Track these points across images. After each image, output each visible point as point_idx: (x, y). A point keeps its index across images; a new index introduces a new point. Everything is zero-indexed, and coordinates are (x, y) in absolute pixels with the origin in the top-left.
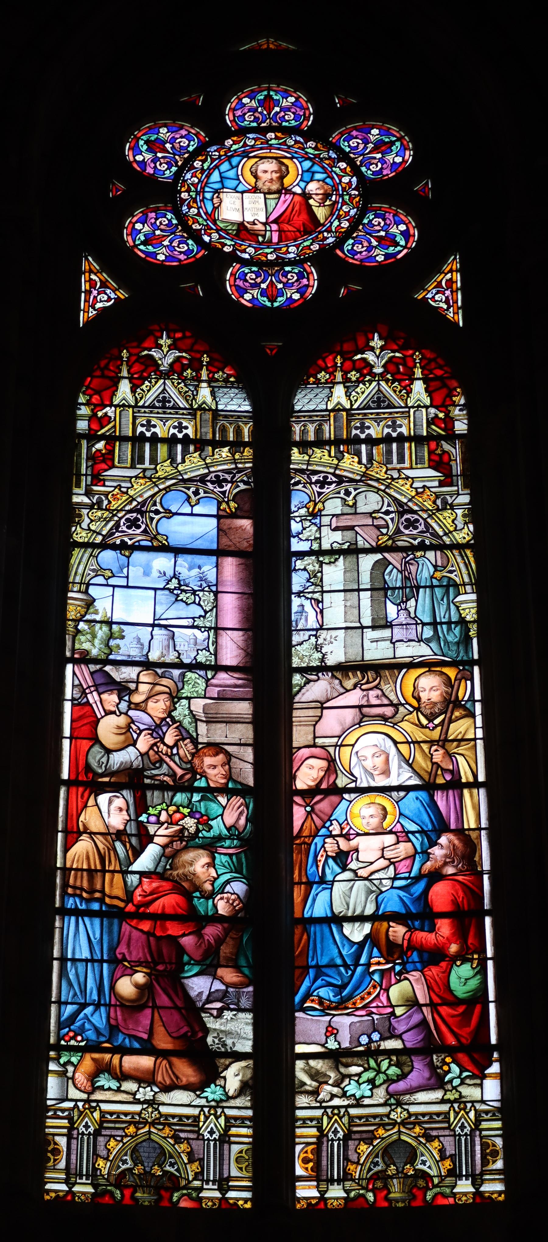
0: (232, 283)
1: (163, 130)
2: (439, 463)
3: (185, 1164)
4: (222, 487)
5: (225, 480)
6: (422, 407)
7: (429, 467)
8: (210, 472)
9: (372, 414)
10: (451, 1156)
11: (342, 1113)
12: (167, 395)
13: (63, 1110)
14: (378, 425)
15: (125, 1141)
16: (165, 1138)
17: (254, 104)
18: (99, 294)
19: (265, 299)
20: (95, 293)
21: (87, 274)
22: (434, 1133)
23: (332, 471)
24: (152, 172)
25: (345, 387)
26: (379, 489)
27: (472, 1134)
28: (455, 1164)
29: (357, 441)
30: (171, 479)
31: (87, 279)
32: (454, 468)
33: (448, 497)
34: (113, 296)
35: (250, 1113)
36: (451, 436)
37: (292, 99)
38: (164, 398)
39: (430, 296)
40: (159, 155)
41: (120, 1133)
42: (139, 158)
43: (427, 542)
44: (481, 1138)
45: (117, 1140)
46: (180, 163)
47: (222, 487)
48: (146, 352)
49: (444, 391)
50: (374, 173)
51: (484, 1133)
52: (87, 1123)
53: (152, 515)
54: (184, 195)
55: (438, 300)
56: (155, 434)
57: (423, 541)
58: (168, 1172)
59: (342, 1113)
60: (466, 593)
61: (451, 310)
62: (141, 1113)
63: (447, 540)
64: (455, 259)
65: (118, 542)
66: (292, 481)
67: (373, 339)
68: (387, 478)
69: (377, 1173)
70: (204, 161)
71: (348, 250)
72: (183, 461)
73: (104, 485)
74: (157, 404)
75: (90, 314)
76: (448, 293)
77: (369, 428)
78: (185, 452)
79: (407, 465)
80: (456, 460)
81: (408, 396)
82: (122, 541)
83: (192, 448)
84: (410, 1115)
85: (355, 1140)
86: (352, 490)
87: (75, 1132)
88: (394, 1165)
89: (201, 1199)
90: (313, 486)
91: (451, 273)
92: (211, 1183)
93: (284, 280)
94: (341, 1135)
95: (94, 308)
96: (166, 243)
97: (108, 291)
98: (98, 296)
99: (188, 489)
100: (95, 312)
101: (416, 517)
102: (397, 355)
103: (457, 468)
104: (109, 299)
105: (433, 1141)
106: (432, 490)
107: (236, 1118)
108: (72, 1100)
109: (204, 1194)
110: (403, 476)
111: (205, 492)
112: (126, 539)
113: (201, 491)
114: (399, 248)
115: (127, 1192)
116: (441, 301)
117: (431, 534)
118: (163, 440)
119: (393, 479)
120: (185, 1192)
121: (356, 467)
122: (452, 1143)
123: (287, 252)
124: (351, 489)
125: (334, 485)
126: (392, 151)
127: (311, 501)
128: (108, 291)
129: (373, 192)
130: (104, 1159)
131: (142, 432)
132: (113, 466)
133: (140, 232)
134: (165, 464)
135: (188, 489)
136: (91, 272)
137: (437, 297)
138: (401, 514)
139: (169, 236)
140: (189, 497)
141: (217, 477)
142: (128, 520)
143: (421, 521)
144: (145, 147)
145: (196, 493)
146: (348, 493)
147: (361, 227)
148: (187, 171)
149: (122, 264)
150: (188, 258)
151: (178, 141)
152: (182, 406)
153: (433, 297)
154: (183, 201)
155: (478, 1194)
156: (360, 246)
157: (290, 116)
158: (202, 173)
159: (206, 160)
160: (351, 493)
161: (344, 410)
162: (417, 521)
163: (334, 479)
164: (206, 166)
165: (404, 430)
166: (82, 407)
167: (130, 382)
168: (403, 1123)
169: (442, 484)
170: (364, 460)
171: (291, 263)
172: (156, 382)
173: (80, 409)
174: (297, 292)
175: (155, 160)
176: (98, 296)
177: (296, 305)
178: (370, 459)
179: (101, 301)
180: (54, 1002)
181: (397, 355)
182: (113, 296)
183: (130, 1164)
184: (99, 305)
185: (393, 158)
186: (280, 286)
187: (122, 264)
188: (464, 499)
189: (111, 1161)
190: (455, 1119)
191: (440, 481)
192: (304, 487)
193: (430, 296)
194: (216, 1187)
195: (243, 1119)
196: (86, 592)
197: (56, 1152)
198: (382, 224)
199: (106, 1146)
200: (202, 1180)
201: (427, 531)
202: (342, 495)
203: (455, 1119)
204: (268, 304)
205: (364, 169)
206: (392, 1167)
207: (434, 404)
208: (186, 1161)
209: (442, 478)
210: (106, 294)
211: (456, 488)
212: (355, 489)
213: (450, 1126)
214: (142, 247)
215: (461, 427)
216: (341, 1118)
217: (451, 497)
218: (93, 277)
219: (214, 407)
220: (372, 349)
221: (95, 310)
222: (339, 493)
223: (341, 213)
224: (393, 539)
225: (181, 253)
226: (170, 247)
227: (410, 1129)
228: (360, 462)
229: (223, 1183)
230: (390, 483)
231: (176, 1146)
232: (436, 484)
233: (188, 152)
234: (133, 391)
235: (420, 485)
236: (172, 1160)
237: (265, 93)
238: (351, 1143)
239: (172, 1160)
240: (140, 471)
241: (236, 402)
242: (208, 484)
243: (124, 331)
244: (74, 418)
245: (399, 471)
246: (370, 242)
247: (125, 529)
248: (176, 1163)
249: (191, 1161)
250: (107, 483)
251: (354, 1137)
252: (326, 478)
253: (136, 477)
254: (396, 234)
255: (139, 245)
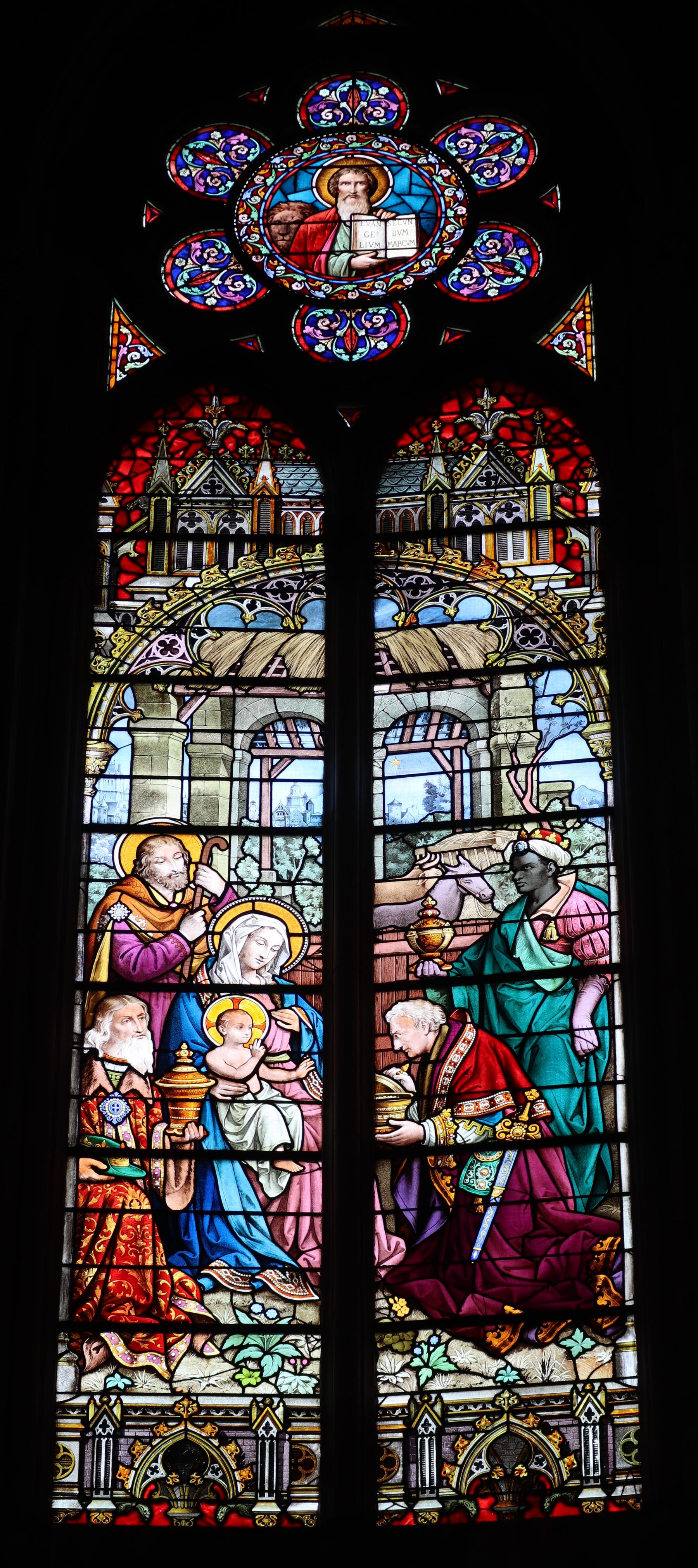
0: (299, 333)
1: (492, 293)
2: (567, 556)
3: (233, 1471)
4: (286, 597)
5: (290, 589)
6: (545, 484)
7: (554, 563)
8: (270, 579)
9: (481, 495)
10: (251, 1464)
11: (112, 1402)
12: (216, 479)
13: (74, 1408)
14: (212, 517)
15: (154, 1443)
16: (207, 1438)
17: (334, 97)
18: (129, 351)
19: (342, 351)
20: (124, 351)
21: (116, 326)
22: (553, 1423)
23: (428, 571)
24: (202, 189)
25: (445, 460)
26: (488, 594)
27: (279, 1438)
28: (255, 1475)
29: (461, 532)
30: (221, 589)
31: (116, 332)
32: (587, 562)
33: (576, 601)
34: (147, 354)
35: (314, 1403)
36: (584, 524)
37: (319, 348)
38: (488, 474)
39: (556, 342)
40: (498, 259)
41: (146, 1433)
42: (184, 173)
43: (549, 659)
44: (292, 1443)
45: (143, 1443)
46: (237, 176)
47: (287, 597)
48: (191, 425)
49: (574, 461)
50: (488, 181)
51: (296, 1438)
52: (105, 1421)
53: (194, 636)
54: (243, 218)
55: (564, 346)
56: (199, 529)
57: (544, 658)
58: (210, 1480)
59: (596, 1388)
60: (597, 721)
61: (584, 359)
62: (174, 1406)
63: (574, 656)
64: (588, 290)
65: (148, 672)
66: (378, 586)
67: (482, 397)
68: (501, 579)
69: (154, 1482)
70: (266, 177)
71: (453, 282)
72: (236, 566)
73: (132, 599)
74: (479, 483)
75: (119, 379)
76: (580, 336)
77: (199, 520)
78: (239, 553)
79: (526, 559)
80: (590, 552)
81: (526, 470)
82: (154, 671)
83: (247, 548)
84: (200, 1408)
85: (450, 1434)
86: (455, 596)
87: (90, 1434)
88: (502, 1466)
89: (255, 1514)
90: (404, 592)
91: (582, 311)
92: (428, 1491)
93: (368, 325)
94: (433, 1428)
95: (122, 369)
96: (217, 282)
97: (141, 348)
98: (132, 354)
99: (242, 601)
100: (124, 376)
101: (536, 627)
102: (512, 416)
103: (590, 561)
104: (143, 358)
105: (551, 1433)
106: (556, 592)
107: (299, 1410)
108: (87, 1393)
109: (257, 1508)
110: (519, 574)
111: (263, 604)
112: (159, 668)
113: (258, 604)
114: (518, 279)
115: (160, 1510)
116: (571, 348)
117: (555, 649)
118: (210, 538)
119: (508, 579)
120: (232, 1506)
121: (457, 563)
122: (253, 1448)
123: (373, 288)
124: (453, 595)
125: (430, 590)
126: (512, 151)
127: (400, 611)
128: (141, 348)
129: (484, 208)
130: (127, 1467)
131: (183, 528)
132: (145, 574)
133: (182, 269)
134: (212, 571)
135: (242, 601)
136: (121, 323)
137: (565, 344)
138: (517, 625)
139: (218, 272)
140: (243, 612)
141: (280, 584)
142: (162, 643)
143: (543, 633)
144: (191, 158)
145: (252, 606)
146: (449, 600)
147: (470, 252)
148: (246, 190)
149: (159, 315)
150: (245, 300)
151: (234, 148)
152: (236, 493)
153: (561, 344)
154: (240, 226)
155: (284, 1514)
156: (469, 277)
157: (379, 113)
158: (265, 191)
159: (270, 174)
160: (452, 599)
161: (445, 490)
162: (537, 632)
163: (431, 582)
164: (270, 181)
165: (521, 514)
166: (109, 499)
167: (170, 464)
168: (513, 1411)
169: (569, 584)
170: (470, 556)
171: (377, 302)
172: (203, 463)
173: (106, 501)
174: (384, 340)
175: (206, 173)
176: (132, 354)
177: (383, 355)
178: (477, 555)
179: (132, 361)
180: (378, 1213)
181: (512, 416)
182: (147, 354)
183: (162, 1473)
184: (129, 367)
185: (513, 158)
186: (362, 333)
187: (159, 315)
188: (597, 603)
189: (136, 1470)
190: (258, 1417)
191: (567, 580)
192: (393, 593)
193: (556, 342)
194: (273, 1498)
195: (308, 1411)
196: (107, 741)
197: (68, 1459)
198: (499, 247)
199: (129, 1451)
200: (256, 1491)
201: (551, 646)
202: (441, 602)
203: (258, 1417)
204: (346, 358)
205: (475, 176)
206: (499, 1469)
207: (562, 478)
208: (234, 1466)
209: (571, 576)
210: (138, 351)
211: (587, 589)
212: (458, 594)
213: (574, 1412)
214: (186, 290)
215: (594, 506)
216: (595, 1396)
217: (580, 601)
218: (124, 330)
219: (276, 493)
220: (481, 410)
221: (124, 373)
222: (437, 599)
223: (444, 234)
224: (505, 657)
225: (236, 293)
226: (223, 288)
227: (521, 1419)
228: (464, 558)
229: (607, 1483)
230: (503, 585)
231: (222, 1449)
232: (563, 584)
233: (248, 162)
234: (174, 471)
235: (542, 586)
236: (540, 1456)
237: (356, 357)
238: (445, 1438)
239: (540, 1456)
240: (178, 580)
241: (304, 480)
242: (269, 594)
243: (158, 397)
244: (97, 511)
245: (515, 568)
246: (481, 271)
247: (158, 654)
248: (545, 1458)
249: (240, 1467)
250: (137, 596)
251: (447, 1430)
252: (419, 580)
253: (174, 588)
254: (497, 268)
255: (182, 287)
